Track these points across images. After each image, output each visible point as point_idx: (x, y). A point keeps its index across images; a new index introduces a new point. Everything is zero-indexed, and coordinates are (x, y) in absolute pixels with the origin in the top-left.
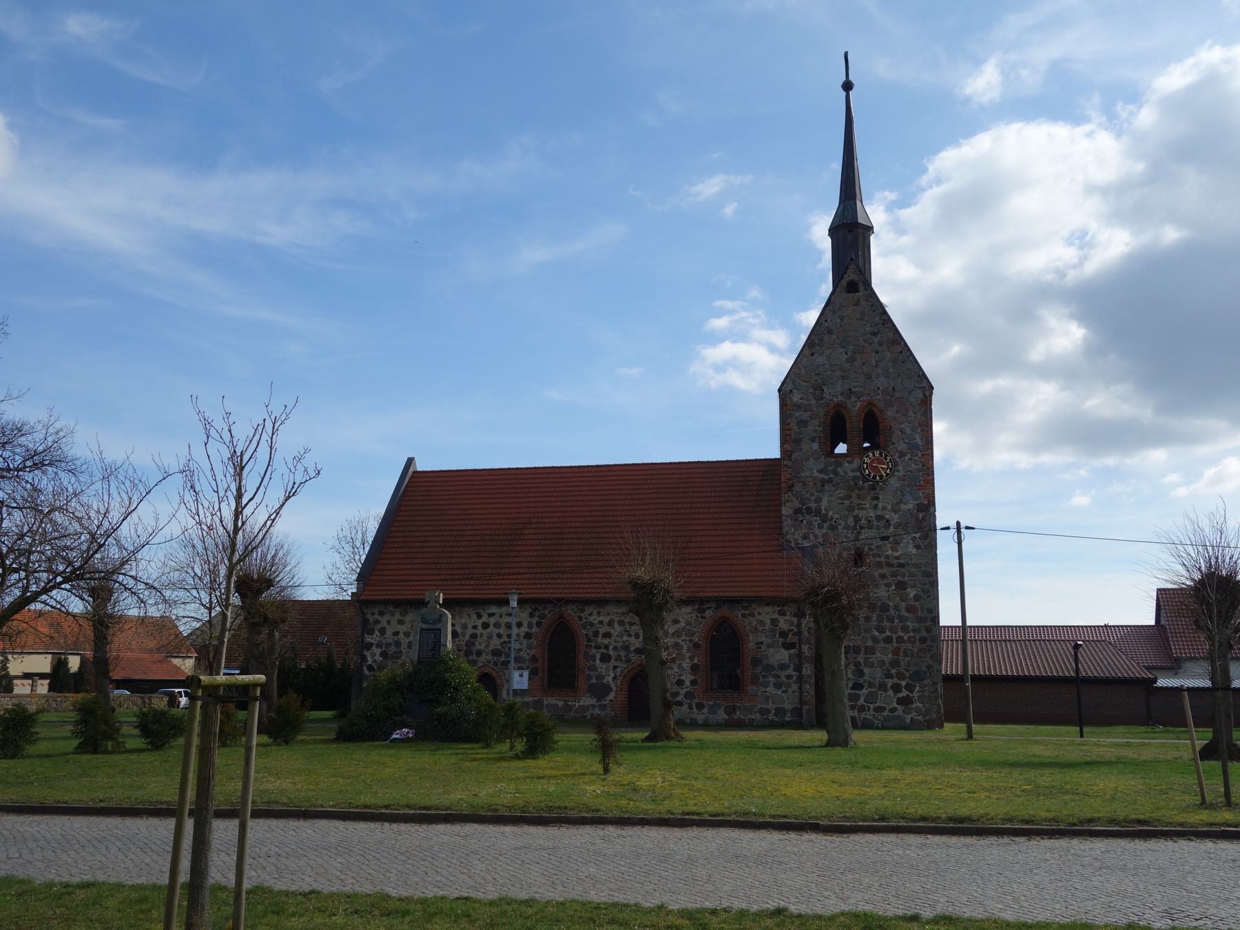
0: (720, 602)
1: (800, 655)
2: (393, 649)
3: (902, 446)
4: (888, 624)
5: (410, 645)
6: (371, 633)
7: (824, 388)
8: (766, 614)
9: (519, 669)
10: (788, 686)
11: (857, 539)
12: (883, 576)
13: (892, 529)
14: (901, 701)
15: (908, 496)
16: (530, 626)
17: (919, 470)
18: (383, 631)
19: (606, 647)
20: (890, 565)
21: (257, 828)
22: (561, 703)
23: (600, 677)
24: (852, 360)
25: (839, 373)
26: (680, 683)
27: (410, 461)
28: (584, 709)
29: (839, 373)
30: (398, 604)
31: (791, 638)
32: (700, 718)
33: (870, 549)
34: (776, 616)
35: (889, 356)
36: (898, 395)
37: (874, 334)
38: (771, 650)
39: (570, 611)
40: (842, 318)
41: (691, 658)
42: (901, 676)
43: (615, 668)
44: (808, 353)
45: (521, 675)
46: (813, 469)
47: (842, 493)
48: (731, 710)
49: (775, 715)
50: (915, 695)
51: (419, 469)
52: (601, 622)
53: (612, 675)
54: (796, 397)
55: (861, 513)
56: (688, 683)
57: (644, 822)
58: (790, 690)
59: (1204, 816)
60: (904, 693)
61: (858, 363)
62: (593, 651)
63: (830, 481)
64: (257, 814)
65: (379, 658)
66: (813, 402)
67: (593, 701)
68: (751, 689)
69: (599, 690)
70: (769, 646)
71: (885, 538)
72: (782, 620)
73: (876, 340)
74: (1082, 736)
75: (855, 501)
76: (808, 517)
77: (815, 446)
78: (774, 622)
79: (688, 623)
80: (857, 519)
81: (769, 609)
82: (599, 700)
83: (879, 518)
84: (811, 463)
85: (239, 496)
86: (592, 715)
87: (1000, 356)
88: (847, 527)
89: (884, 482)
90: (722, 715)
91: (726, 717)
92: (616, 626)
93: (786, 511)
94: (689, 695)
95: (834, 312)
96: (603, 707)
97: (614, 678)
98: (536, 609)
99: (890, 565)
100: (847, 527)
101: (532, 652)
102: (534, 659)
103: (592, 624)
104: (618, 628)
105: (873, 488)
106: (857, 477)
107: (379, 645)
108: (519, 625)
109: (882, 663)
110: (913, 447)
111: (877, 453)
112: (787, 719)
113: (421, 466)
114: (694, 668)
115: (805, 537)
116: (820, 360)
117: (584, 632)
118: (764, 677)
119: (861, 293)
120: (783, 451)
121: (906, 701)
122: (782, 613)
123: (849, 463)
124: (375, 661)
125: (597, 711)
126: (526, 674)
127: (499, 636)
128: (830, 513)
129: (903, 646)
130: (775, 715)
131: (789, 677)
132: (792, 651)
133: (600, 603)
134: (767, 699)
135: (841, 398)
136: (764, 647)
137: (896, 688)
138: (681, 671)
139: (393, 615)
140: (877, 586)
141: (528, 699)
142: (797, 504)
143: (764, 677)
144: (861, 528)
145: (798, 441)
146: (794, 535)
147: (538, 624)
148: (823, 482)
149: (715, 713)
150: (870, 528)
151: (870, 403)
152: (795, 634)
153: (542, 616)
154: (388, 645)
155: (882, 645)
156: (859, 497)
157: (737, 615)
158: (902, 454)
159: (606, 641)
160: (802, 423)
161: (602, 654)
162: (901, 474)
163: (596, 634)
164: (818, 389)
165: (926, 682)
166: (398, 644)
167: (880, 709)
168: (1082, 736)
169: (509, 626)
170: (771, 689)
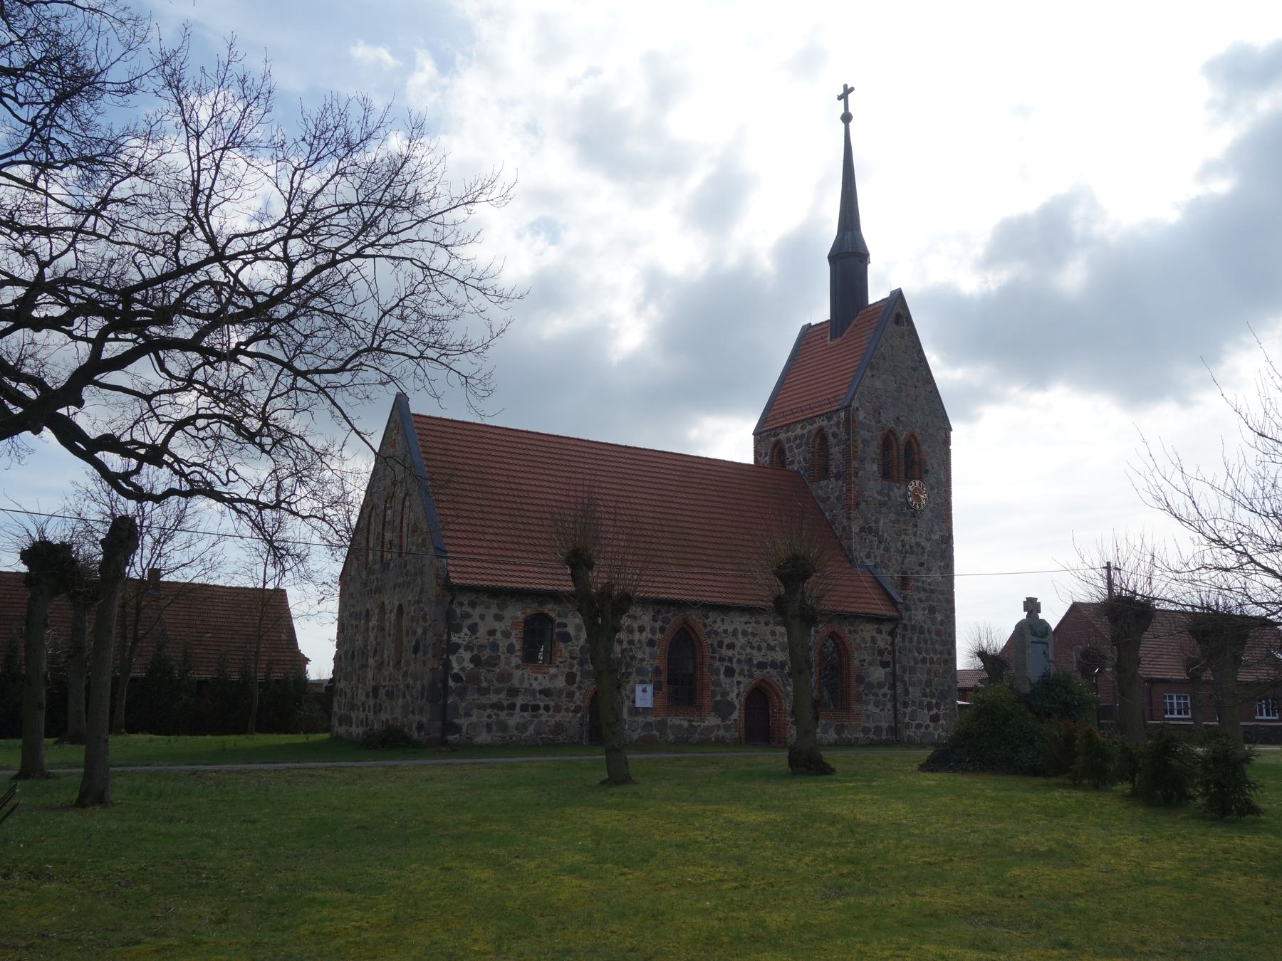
2: (486, 654)
5: (511, 649)
6: (458, 629)
8: (868, 631)
9: (642, 682)
16: (653, 631)
18: (473, 629)
19: (730, 660)
20: (925, 590)
22: (685, 724)
23: (725, 694)
28: (709, 729)
30: (494, 593)
31: (888, 658)
34: (874, 634)
39: (695, 617)
40: (892, 348)
42: (932, 696)
45: (644, 691)
48: (840, 730)
52: (725, 631)
55: (907, 539)
62: (718, 664)
63: (885, 504)
65: (469, 665)
66: (873, 423)
67: (718, 721)
69: (723, 709)
70: (870, 664)
77: (875, 467)
78: (874, 640)
81: (869, 627)
82: (723, 720)
84: (872, 483)
85: (317, 371)
87: (328, 579)
88: (896, 551)
92: (740, 636)
96: (727, 728)
97: (738, 695)
98: (658, 612)
99: (925, 590)
100: (896, 551)
102: (657, 671)
103: (716, 633)
104: (742, 640)
107: (469, 647)
108: (642, 629)
112: (884, 737)
115: (868, 556)
117: (709, 641)
119: (904, 328)
124: (463, 669)
125: (722, 732)
126: (650, 688)
129: (935, 667)
131: (885, 695)
132: (888, 669)
133: (724, 609)
134: (868, 716)
139: (488, 608)
141: (651, 719)
146: (860, 554)
147: (662, 630)
152: (889, 653)
153: (666, 621)
154: (481, 647)
155: (920, 665)
157: (845, 629)
159: (730, 653)
163: (720, 644)
166: (494, 646)
167: (919, 726)
170: (871, 707)
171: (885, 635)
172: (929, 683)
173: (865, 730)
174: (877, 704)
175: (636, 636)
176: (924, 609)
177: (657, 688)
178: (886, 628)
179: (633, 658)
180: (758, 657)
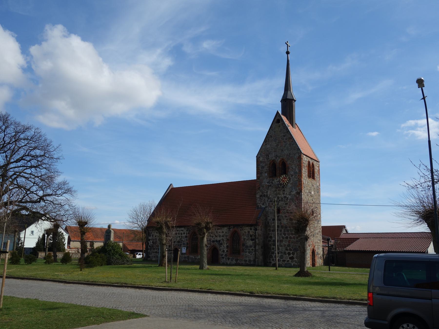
0: (234, 226)
1: (255, 242)
3: (292, 173)
8: (247, 229)
9: (184, 247)
12: (286, 216)
13: (289, 201)
14: (290, 258)
15: (294, 190)
16: (187, 234)
17: (297, 181)
18: (153, 236)
21: (7, 281)
22: (194, 257)
24: (277, 145)
26: (224, 251)
27: (171, 184)
29: (273, 150)
31: (253, 237)
32: (229, 262)
34: (249, 230)
35: (288, 143)
36: (291, 156)
37: (284, 136)
40: (275, 132)
41: (227, 244)
42: (291, 250)
44: (265, 144)
46: (265, 182)
47: (274, 189)
48: (237, 260)
50: (295, 256)
51: (174, 187)
54: (261, 159)
55: (279, 196)
56: (225, 251)
57: (171, 290)
59: (165, 284)
60: (291, 255)
61: (279, 146)
63: (270, 186)
64: (7, 277)
65: (152, 243)
66: (266, 160)
70: (247, 240)
71: (286, 204)
72: (251, 231)
74: (329, 270)
75: (278, 192)
77: (266, 174)
78: (249, 232)
79: (226, 233)
80: (278, 198)
81: (247, 228)
83: (285, 197)
84: (265, 180)
89: (287, 185)
90: (234, 262)
93: (258, 196)
94: (226, 255)
95: (273, 130)
102: (187, 244)
105: (283, 187)
107: (152, 240)
108: (184, 233)
109: (285, 245)
110: (295, 173)
111: (284, 175)
113: (175, 186)
114: (227, 247)
115: (263, 204)
116: (268, 146)
120: (257, 177)
121: (292, 258)
122: (251, 229)
123: (276, 179)
126: (185, 248)
127: (179, 237)
129: (291, 240)
131: (252, 250)
132: (253, 241)
134: (246, 257)
135: (274, 158)
136: (246, 240)
137: (289, 254)
138: (224, 248)
140: (284, 220)
141: (186, 256)
142: (261, 194)
144: (280, 201)
145: (261, 173)
147: (189, 233)
148: (269, 186)
149: (232, 261)
150: (282, 201)
151: (283, 159)
154: (154, 239)
155: (285, 239)
156: (279, 190)
158: (292, 175)
160: (263, 167)
162: (292, 182)
165: (298, 252)
166: (156, 239)
167: (284, 261)
168: (329, 270)
169: (182, 234)
170: (247, 254)
171: (253, 230)
172: (289, 246)
173: (245, 261)
174: (249, 252)
175: (183, 235)
176: (287, 220)
177: (187, 248)
178: (253, 228)
179: (182, 241)
180: (212, 239)
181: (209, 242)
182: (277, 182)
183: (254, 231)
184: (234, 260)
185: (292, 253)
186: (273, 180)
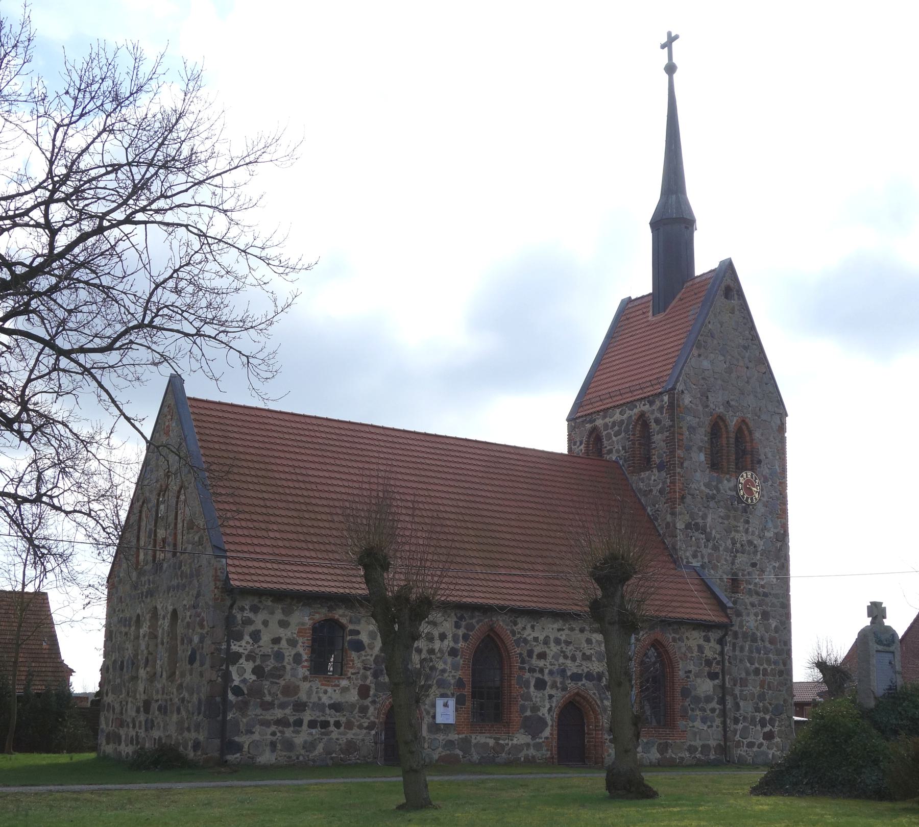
2: (270, 664)
4: (757, 655)
5: (297, 659)
6: (239, 637)
7: (709, 394)
8: (694, 638)
9: (443, 696)
10: (713, 721)
11: (733, 563)
12: (753, 605)
13: (759, 557)
16: (455, 639)
18: (256, 636)
19: (541, 671)
20: (757, 594)
22: (491, 742)
25: (719, 382)
28: (518, 748)
30: (279, 596)
31: (716, 668)
33: (743, 575)
34: (701, 642)
38: (699, 680)
42: (766, 711)
43: (551, 697)
45: (446, 705)
49: (701, 753)
53: (548, 706)
55: (737, 536)
58: (714, 725)
62: (527, 675)
63: (713, 497)
65: (250, 677)
66: (700, 408)
68: (681, 723)
69: (534, 726)
70: (697, 676)
73: (747, 355)
76: (696, 534)
77: (702, 457)
78: (701, 649)
80: (734, 543)
81: (695, 634)
82: (533, 738)
84: (698, 474)
86: (526, 757)
88: (726, 549)
91: (658, 756)
92: (552, 644)
96: (538, 747)
97: (550, 710)
98: (461, 618)
99: (757, 594)
100: (726, 549)
101: (459, 674)
102: (460, 684)
103: (526, 641)
106: (732, 496)
107: (250, 657)
108: (443, 637)
118: (692, 710)
119: (735, 302)
123: (729, 481)
124: (244, 681)
125: (532, 752)
126: (452, 702)
128: (714, 532)
129: (769, 678)
130: (701, 753)
131: (713, 710)
133: (535, 614)
134: (695, 734)
136: (692, 676)
139: (272, 613)
141: (454, 737)
143: (692, 710)
147: (465, 637)
152: (718, 663)
153: (470, 628)
154: (265, 657)
155: (752, 677)
157: (668, 637)
159: (541, 663)
161: (538, 679)
163: (530, 653)
164: (705, 395)
166: (279, 656)
167: (751, 745)
170: (698, 724)
171: (712, 643)
172: (762, 697)
173: (692, 749)
174: (704, 720)
176: (756, 615)
177: (460, 702)
178: (714, 635)
180: (572, 668)
181: (559, 680)
182: (730, 489)
183: (718, 647)
184: (654, 750)
185: (771, 719)
186: (720, 481)
